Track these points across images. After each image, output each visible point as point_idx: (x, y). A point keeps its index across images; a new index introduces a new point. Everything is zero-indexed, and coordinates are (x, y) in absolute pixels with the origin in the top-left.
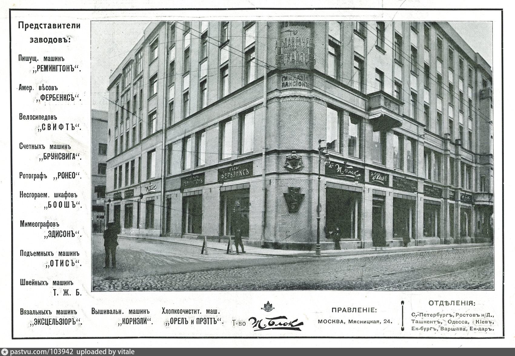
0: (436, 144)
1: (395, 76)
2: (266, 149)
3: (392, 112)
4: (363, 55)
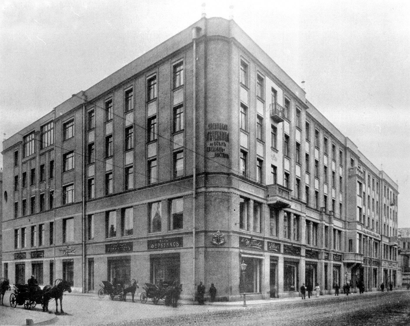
3: (284, 198)
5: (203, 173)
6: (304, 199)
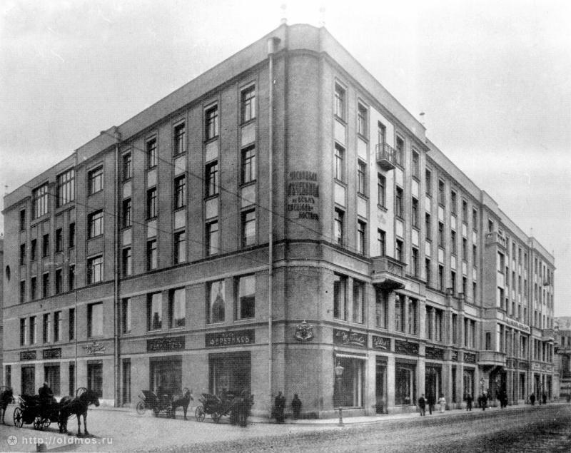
0: (438, 301)
1: (413, 242)
2: (273, 318)
4: (401, 236)
5: (283, 241)
6: (423, 276)
